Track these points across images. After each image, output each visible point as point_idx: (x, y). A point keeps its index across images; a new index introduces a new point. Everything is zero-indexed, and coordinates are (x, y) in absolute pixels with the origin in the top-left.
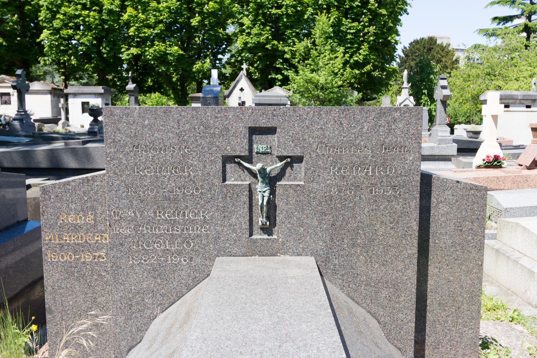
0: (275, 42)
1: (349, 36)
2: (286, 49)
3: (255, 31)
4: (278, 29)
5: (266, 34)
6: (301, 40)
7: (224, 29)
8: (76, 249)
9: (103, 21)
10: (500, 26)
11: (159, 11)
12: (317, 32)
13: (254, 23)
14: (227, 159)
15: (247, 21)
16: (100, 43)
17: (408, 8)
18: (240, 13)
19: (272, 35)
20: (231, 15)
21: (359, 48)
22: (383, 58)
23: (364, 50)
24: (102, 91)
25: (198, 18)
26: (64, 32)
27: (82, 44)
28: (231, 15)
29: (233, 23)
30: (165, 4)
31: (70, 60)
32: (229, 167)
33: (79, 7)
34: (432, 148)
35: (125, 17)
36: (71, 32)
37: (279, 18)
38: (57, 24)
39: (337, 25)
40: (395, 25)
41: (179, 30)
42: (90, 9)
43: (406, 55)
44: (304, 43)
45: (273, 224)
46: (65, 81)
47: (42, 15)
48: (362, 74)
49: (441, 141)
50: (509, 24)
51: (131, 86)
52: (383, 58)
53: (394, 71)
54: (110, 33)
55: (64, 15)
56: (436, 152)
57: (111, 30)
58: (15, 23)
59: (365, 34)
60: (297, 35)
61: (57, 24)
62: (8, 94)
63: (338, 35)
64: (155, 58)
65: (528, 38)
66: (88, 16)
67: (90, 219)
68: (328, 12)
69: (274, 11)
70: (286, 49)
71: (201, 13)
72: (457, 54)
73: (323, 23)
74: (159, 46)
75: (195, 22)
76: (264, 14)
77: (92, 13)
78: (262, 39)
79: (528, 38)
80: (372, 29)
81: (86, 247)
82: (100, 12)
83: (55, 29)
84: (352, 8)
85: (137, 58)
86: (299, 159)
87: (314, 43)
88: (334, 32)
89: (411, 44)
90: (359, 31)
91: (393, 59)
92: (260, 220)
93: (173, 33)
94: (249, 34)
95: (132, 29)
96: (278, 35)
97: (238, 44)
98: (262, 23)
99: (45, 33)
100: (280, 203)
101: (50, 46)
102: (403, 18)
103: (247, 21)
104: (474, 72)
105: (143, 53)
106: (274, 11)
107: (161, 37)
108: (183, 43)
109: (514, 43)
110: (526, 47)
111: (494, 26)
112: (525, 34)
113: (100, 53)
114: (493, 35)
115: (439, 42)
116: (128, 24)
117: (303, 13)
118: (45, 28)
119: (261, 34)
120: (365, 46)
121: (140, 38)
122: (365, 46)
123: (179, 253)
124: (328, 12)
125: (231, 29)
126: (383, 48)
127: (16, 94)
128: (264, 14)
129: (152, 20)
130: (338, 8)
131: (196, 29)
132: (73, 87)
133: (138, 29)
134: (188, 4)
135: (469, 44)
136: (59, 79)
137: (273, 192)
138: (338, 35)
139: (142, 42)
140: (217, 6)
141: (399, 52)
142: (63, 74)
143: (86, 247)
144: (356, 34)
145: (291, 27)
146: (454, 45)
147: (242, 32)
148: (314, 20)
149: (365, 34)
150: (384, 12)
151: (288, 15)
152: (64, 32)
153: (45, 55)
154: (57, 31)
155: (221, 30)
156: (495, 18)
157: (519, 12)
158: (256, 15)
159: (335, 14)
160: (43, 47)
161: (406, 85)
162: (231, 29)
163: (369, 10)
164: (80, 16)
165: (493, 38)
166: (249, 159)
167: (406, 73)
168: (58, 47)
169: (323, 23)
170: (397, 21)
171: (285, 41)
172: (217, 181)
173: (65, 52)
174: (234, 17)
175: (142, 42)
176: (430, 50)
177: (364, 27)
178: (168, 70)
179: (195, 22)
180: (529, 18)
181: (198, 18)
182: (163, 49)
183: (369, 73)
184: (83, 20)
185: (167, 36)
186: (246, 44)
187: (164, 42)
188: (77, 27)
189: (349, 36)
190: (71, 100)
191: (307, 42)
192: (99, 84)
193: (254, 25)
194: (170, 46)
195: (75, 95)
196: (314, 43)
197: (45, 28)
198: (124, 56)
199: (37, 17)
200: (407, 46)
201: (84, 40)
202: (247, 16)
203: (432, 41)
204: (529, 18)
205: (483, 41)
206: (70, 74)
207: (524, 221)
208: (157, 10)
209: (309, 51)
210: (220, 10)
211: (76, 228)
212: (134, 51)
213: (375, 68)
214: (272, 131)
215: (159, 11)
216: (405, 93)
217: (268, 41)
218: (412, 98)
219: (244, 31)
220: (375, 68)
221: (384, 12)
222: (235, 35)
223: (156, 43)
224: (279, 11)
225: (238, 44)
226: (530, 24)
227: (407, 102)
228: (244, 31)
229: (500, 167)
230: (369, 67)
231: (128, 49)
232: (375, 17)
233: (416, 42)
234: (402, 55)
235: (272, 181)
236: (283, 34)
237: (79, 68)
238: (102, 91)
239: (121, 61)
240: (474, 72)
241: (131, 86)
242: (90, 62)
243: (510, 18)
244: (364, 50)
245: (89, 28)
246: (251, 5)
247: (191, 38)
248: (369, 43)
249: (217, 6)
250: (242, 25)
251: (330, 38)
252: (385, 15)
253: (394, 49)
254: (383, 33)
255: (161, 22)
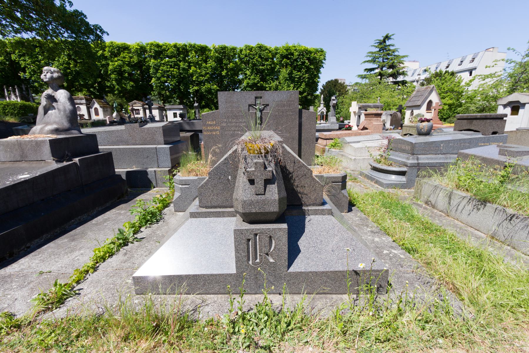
0: (262, 83)
1: (296, 79)
2: (267, 86)
3: (252, 77)
4: (263, 76)
5: (258, 79)
6: (274, 81)
7: (238, 77)
8: (211, 131)
9: (181, 74)
10: (368, 73)
11: (207, 68)
12: (281, 77)
13: (252, 73)
14: (250, 105)
15: (248, 73)
16: (179, 85)
17: (324, 65)
18: (245, 69)
19: (260, 79)
20: (241, 70)
21: (301, 85)
22: (312, 89)
23: (303, 86)
24: (182, 107)
25: (225, 71)
26: (162, 79)
27: (171, 85)
28: (241, 70)
29: (242, 74)
30: (209, 65)
31: (165, 93)
32: (250, 108)
33: (169, 66)
34: (328, 126)
35: (191, 71)
36: (165, 79)
37: (263, 70)
38: (158, 75)
39: (290, 74)
40: (318, 74)
41: (217, 77)
42: (174, 68)
43: (324, 89)
44: (275, 83)
45: (262, 123)
46: (164, 103)
47: (151, 71)
48: (302, 97)
49: (332, 123)
50: (372, 72)
51: (196, 104)
52: (312, 89)
53: (317, 95)
54: (184, 80)
55: (162, 70)
56: (330, 128)
57: (184, 78)
58: (139, 75)
59: (303, 78)
60: (272, 79)
61: (158, 75)
62: (138, 110)
63: (291, 78)
64: (206, 91)
65: (381, 79)
66: (173, 71)
67: (214, 123)
68: (286, 67)
69: (261, 67)
70: (267, 86)
71: (227, 69)
72: (348, 88)
73: (284, 73)
74: (208, 85)
75: (224, 73)
76: (256, 69)
77: (175, 70)
78: (256, 81)
79: (381, 79)
80: (307, 75)
81: (214, 130)
82: (179, 69)
83: (158, 78)
84: (297, 65)
85: (197, 91)
86: (268, 105)
87: (280, 83)
88: (289, 77)
89: (326, 83)
90: (301, 77)
91: (317, 90)
92: (258, 121)
93: (214, 78)
94: (249, 79)
95: (194, 77)
96: (263, 79)
97: (245, 84)
98: (255, 74)
99: (153, 80)
100: (263, 117)
101: (156, 86)
102: (322, 70)
103: (248, 73)
104: (355, 96)
105: (200, 89)
106: (261, 67)
107: (208, 81)
108: (218, 84)
109: (373, 82)
110: (380, 83)
111: (365, 73)
112: (379, 77)
113: (180, 89)
114: (364, 78)
115: (339, 82)
116: (192, 75)
117: (275, 68)
118: (153, 77)
119: (255, 79)
120: (304, 84)
121: (198, 81)
122: (304, 84)
123: (238, 131)
124: (286, 67)
125: (241, 77)
126: (312, 85)
127: (142, 110)
128: (256, 69)
129: (204, 73)
130: (291, 65)
131: (224, 77)
132: (167, 106)
133: (197, 77)
134: (220, 65)
135: (353, 83)
136: (161, 103)
137: (261, 114)
138: (291, 78)
139: (200, 84)
140: (234, 65)
141: (320, 87)
142: (162, 100)
143: (214, 130)
144: (299, 78)
145: (269, 75)
146: (347, 83)
147: (246, 78)
148: (280, 71)
149: (303, 78)
150: (312, 67)
151: (267, 69)
152: (162, 79)
153: (154, 91)
154: (159, 79)
155: (236, 77)
156: (366, 69)
157: (377, 66)
158: (253, 70)
159: (289, 68)
160: (153, 87)
161: (322, 102)
162: (241, 77)
163: (305, 66)
164: (169, 71)
165: (364, 79)
166: (255, 105)
167: (322, 96)
168: (160, 86)
169: (284, 73)
170: (318, 72)
171: (266, 82)
172: (247, 111)
173: (163, 89)
174: (242, 71)
175: (200, 84)
176: (335, 86)
177: (303, 74)
178: (212, 97)
179: (224, 73)
180: (382, 69)
181: (225, 71)
182: (209, 86)
183: (306, 97)
184: (171, 73)
185: (211, 80)
186: (248, 83)
187: (210, 83)
188: (168, 77)
189: (296, 79)
190: (168, 112)
191: (276, 82)
192: (180, 104)
193: (252, 74)
194: (213, 85)
195: (170, 109)
196: (280, 83)
197: (153, 77)
198: (191, 91)
199: (149, 72)
200: (325, 84)
201: (172, 83)
202: (248, 70)
203: (336, 81)
204: (382, 69)
205: (359, 80)
206: (166, 100)
207: (353, 145)
208: (206, 68)
209: (278, 86)
210: (235, 67)
211: (211, 125)
212: (196, 88)
213: (308, 95)
214: (261, 98)
215: (207, 68)
216: (322, 106)
217: (258, 82)
218: (325, 108)
219: (247, 77)
220: (308, 95)
221: (312, 67)
222: (243, 79)
223: (206, 84)
224: (263, 67)
225: (245, 84)
226: (382, 72)
227: (323, 110)
228: (247, 77)
229: (351, 130)
230: (305, 94)
231: (193, 87)
232: (308, 70)
233: (329, 82)
234: (322, 88)
235: (261, 111)
236: (265, 78)
237: (171, 97)
238: (182, 107)
239: (190, 93)
240: (355, 96)
241: (196, 104)
242: (175, 94)
243: (373, 69)
244: (303, 86)
245: (174, 77)
246: (250, 64)
247: (222, 81)
248: (305, 82)
249: (234, 65)
250: (246, 74)
251: (288, 80)
252: (312, 69)
253: (317, 85)
254: (312, 77)
255: (208, 73)
